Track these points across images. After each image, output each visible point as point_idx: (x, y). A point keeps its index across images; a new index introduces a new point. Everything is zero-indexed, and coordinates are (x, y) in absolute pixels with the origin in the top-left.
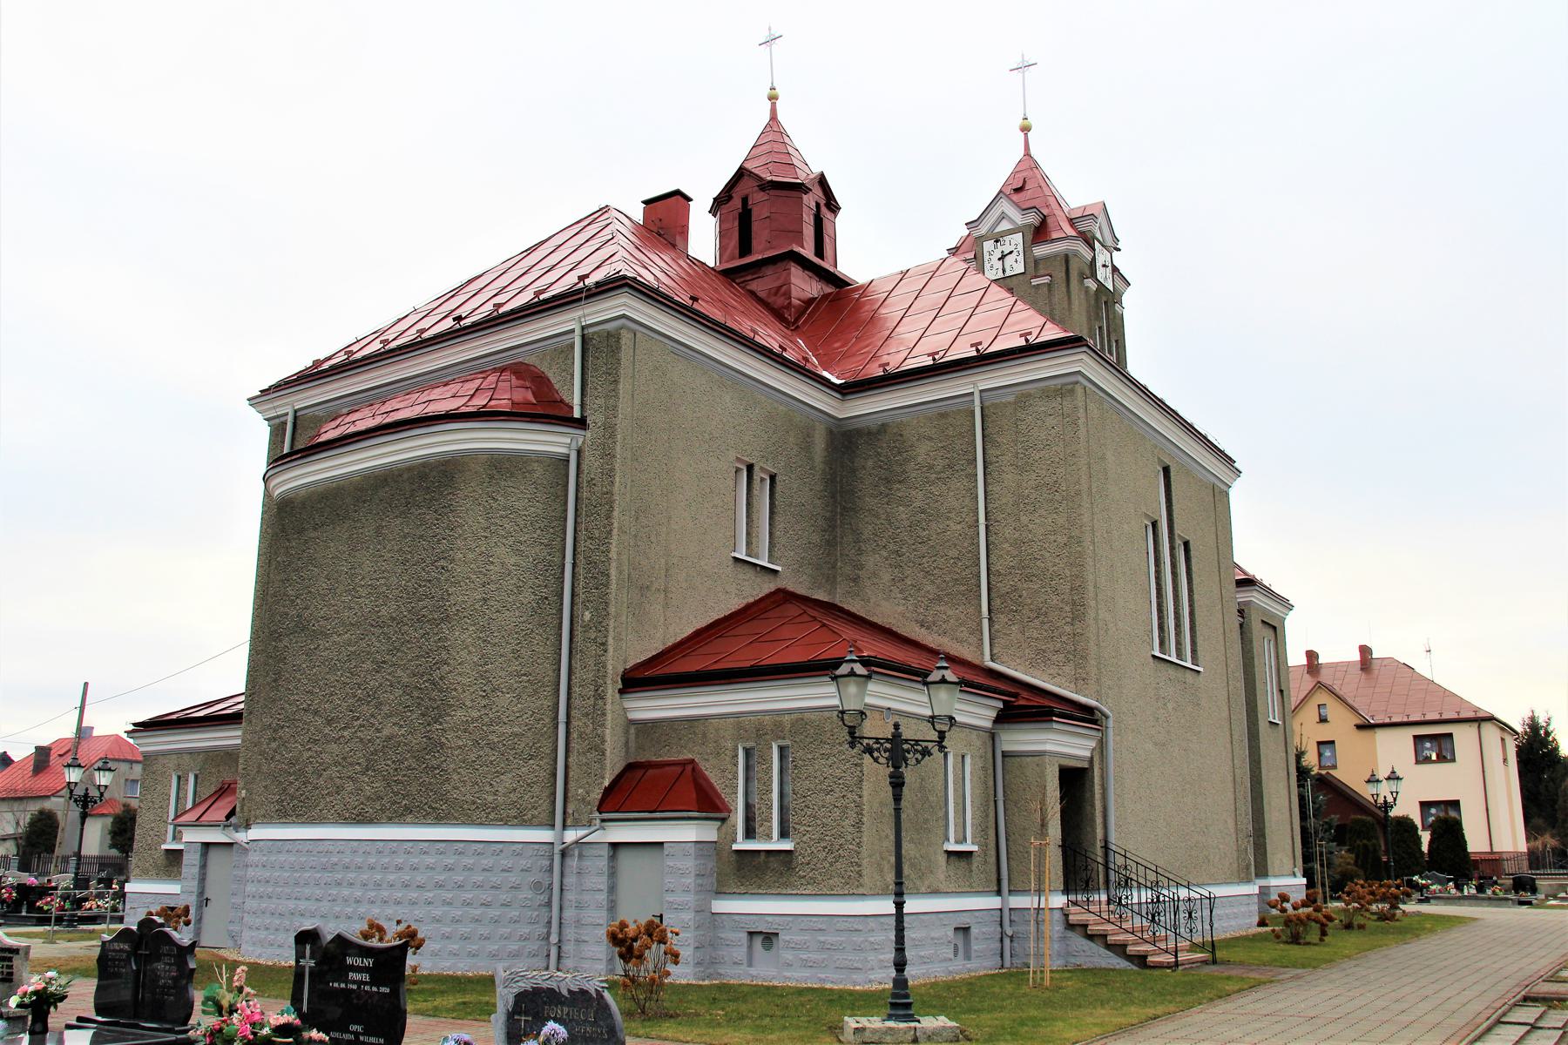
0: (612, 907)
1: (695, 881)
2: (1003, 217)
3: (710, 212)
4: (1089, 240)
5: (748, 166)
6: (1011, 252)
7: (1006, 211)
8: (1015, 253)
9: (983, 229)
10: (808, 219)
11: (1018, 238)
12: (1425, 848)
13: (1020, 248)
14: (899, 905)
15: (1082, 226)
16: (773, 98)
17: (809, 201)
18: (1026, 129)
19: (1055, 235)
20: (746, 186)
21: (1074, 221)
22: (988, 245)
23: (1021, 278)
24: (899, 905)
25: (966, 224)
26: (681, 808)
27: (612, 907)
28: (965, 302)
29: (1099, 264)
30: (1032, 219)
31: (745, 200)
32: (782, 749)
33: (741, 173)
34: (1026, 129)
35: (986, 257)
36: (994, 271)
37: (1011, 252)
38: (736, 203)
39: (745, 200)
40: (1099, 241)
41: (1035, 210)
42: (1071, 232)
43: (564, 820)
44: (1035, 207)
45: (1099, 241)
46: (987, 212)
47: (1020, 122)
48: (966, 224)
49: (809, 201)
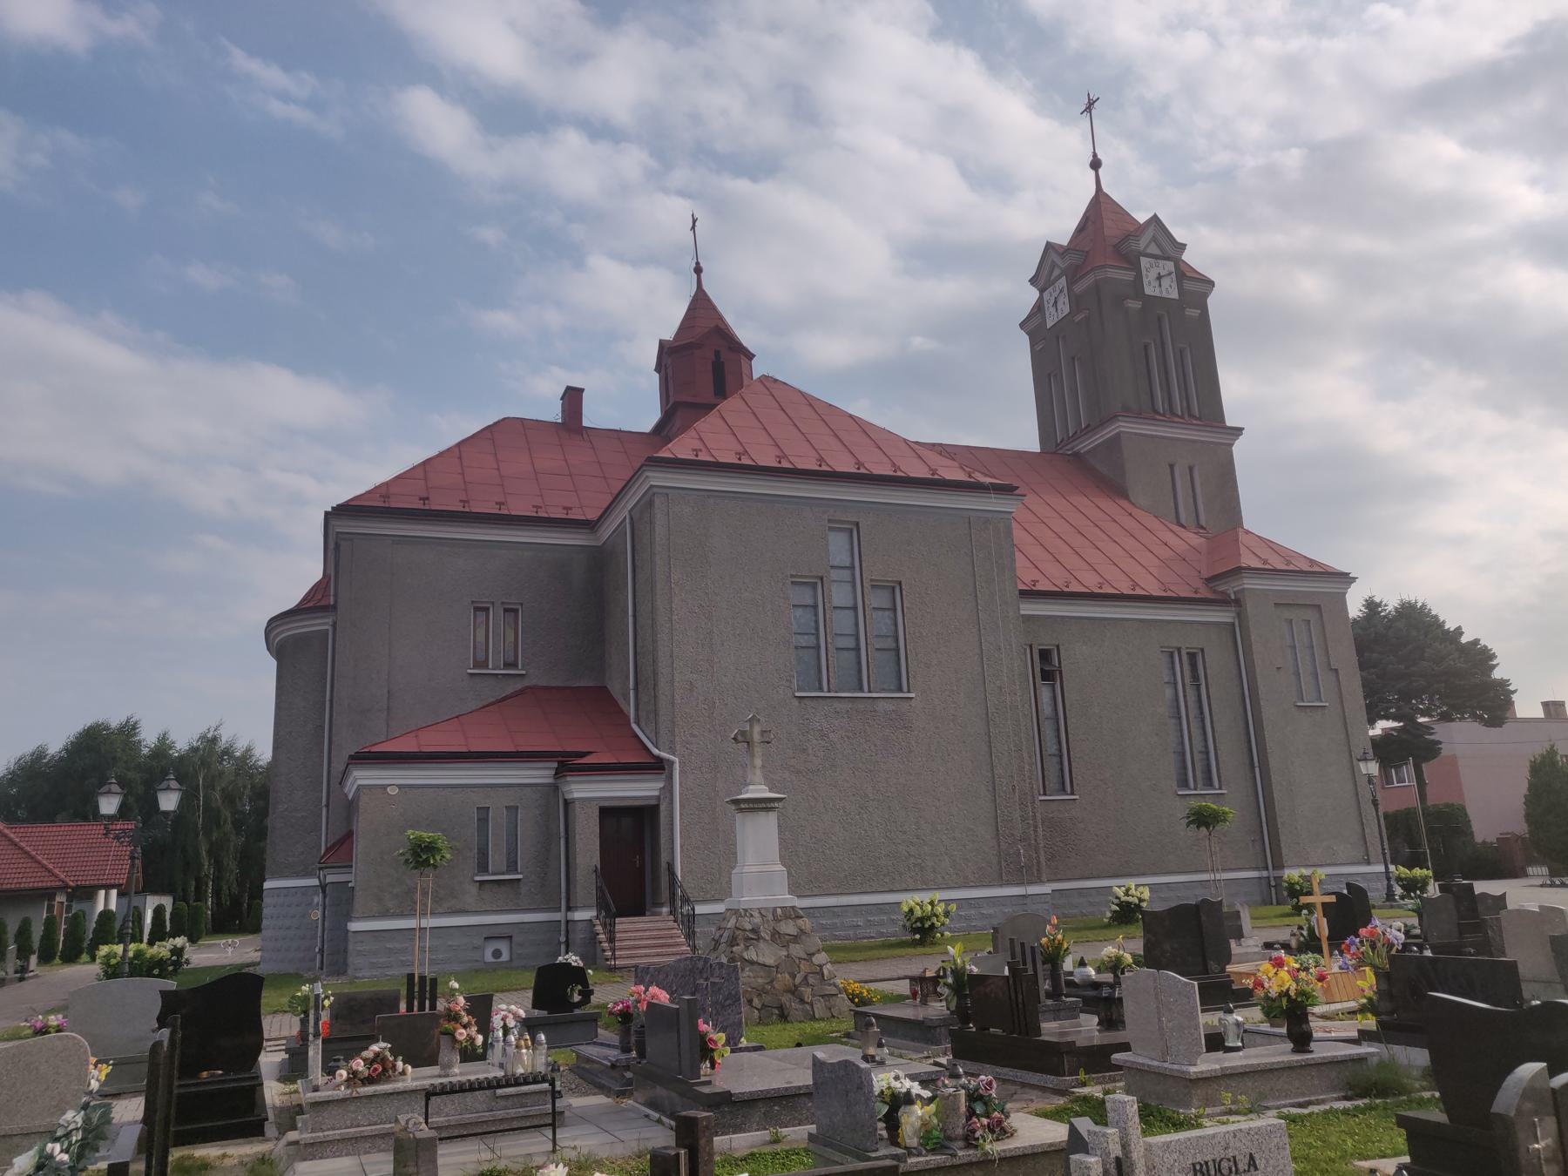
16: (698, 270)
31: (717, 354)
32: (519, 880)
39: (717, 354)
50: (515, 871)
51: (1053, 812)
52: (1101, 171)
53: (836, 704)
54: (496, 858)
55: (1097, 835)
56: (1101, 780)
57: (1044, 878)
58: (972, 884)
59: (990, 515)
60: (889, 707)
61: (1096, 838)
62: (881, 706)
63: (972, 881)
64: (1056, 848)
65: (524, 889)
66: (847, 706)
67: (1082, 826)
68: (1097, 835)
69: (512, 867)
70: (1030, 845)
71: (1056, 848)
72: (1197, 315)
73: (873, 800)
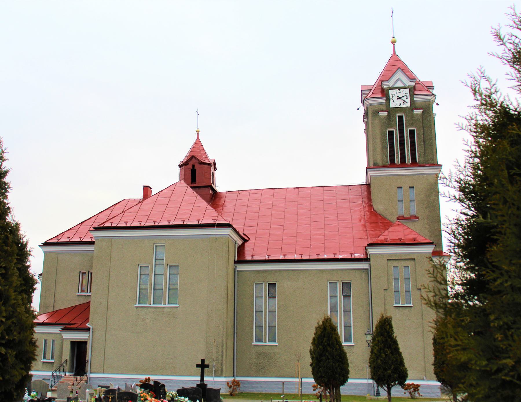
0: (209, 384)
2: (399, 79)
3: (180, 166)
6: (403, 97)
7: (401, 78)
8: (405, 97)
11: (407, 91)
13: (408, 95)
14: (202, 379)
16: (198, 132)
18: (393, 42)
20: (193, 161)
24: (202, 379)
26: (160, 237)
27: (209, 384)
28: (328, 219)
31: (193, 166)
32: (277, 345)
34: (393, 42)
35: (391, 97)
37: (403, 97)
38: (190, 166)
39: (193, 166)
43: (139, 301)
47: (391, 39)
50: (274, 341)
51: (265, 350)
52: (396, 45)
53: (149, 309)
54: (49, 355)
55: (285, 360)
56: (290, 338)
57: (224, 375)
58: (194, 375)
59: (216, 236)
60: (169, 310)
61: (285, 361)
62: (165, 310)
63: (194, 374)
64: (265, 364)
65: (55, 365)
66: (154, 310)
67: (279, 356)
68: (285, 360)
69: (52, 358)
70: (219, 362)
71: (265, 364)
72: (421, 112)
73: (159, 343)
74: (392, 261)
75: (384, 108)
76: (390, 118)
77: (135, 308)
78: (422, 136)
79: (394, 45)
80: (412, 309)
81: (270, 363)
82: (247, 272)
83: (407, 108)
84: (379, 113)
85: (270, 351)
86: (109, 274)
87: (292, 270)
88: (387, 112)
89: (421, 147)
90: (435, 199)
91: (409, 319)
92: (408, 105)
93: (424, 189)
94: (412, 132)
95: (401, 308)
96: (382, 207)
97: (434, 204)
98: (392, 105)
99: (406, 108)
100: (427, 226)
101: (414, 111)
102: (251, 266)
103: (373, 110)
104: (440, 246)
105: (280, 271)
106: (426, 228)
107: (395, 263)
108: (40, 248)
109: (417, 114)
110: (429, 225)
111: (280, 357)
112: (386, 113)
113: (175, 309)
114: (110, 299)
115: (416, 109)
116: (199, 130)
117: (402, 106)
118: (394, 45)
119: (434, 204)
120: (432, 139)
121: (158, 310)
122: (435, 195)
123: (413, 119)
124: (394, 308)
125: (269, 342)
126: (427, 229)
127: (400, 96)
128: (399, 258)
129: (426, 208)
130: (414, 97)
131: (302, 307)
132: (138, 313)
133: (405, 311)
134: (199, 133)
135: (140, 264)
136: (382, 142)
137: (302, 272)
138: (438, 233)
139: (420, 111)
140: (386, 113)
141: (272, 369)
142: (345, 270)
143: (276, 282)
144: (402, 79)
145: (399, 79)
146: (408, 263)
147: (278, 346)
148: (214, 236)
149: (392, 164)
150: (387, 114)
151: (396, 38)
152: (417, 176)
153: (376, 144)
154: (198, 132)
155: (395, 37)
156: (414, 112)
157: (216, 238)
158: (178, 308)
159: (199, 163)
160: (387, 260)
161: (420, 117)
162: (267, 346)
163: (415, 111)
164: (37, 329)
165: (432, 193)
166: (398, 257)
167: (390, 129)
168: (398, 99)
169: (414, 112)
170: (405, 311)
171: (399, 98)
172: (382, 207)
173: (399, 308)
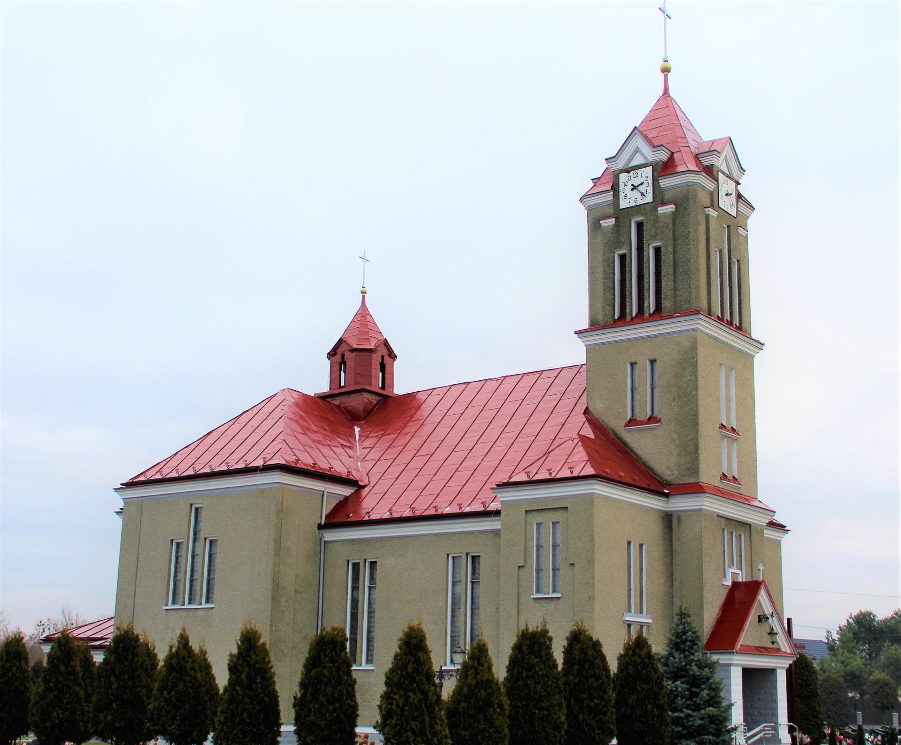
1: (610, 696)
2: (637, 151)
4: (709, 171)
5: (344, 338)
6: (642, 184)
7: (639, 147)
8: (645, 185)
9: (620, 164)
10: (376, 365)
11: (649, 171)
12: (339, 735)
13: (650, 180)
15: (706, 161)
16: (363, 293)
17: (376, 359)
18: (666, 71)
19: (680, 169)
21: (699, 156)
22: (623, 177)
23: (651, 204)
25: (605, 160)
29: (722, 194)
30: (663, 156)
31: (343, 356)
32: (373, 670)
33: (341, 342)
34: (666, 71)
35: (621, 187)
36: (628, 200)
37: (642, 184)
39: (343, 356)
40: (723, 173)
41: (663, 148)
42: (693, 167)
44: (662, 145)
45: (723, 173)
46: (621, 151)
47: (660, 64)
48: (605, 160)
49: (376, 359)
62: (200, 613)
74: (534, 513)
75: (610, 211)
76: (619, 230)
77: (165, 611)
78: (671, 258)
79: (666, 76)
80: (561, 600)
81: (363, 702)
82: (339, 544)
83: (648, 206)
84: (601, 222)
85: (364, 681)
86: (138, 558)
87: (398, 537)
88: (613, 219)
89: (668, 280)
90: (690, 380)
91: (554, 622)
92: (649, 198)
93: (672, 363)
94: (658, 250)
95: (543, 601)
96: (601, 405)
97: (688, 391)
98: (623, 204)
99: (645, 205)
100: (675, 436)
101: (658, 209)
102: (342, 532)
103: (594, 218)
104: (694, 473)
105: (382, 539)
106: (672, 439)
107: (539, 518)
108: (117, 516)
109: (664, 215)
110: (679, 434)
111: (376, 691)
112: (612, 221)
113: (210, 612)
114: (137, 599)
115: (663, 204)
116: (367, 289)
117: (639, 202)
118: (666, 76)
119: (688, 391)
120: (689, 262)
121: (191, 613)
122: (690, 372)
123: (657, 225)
124: (533, 600)
125: (367, 665)
126: (674, 441)
127: (636, 184)
128: (544, 508)
129: (674, 399)
130: (660, 181)
131: (410, 602)
132: (168, 620)
133: (549, 607)
134: (366, 295)
135: (175, 539)
136: (604, 279)
137: (412, 539)
138: (692, 448)
139: (671, 208)
140: (612, 221)
141: (366, 712)
142: (472, 532)
143: (376, 558)
144: (642, 150)
145: (637, 151)
146: (558, 516)
147: (374, 672)
148: (255, 487)
149: (622, 320)
150: (614, 223)
151: (671, 63)
152: (661, 339)
153: (596, 284)
154: (363, 293)
155: (668, 59)
156: (659, 212)
157: (261, 491)
158: (214, 611)
159: (350, 351)
160: (526, 511)
161: (669, 221)
162: (361, 672)
163: (662, 210)
164: (743, 581)
165: (685, 369)
166: (543, 506)
167: (654, 243)
168: (632, 190)
169: (659, 212)
170: (549, 607)
171: (634, 188)
172: (601, 405)
173: (539, 601)
